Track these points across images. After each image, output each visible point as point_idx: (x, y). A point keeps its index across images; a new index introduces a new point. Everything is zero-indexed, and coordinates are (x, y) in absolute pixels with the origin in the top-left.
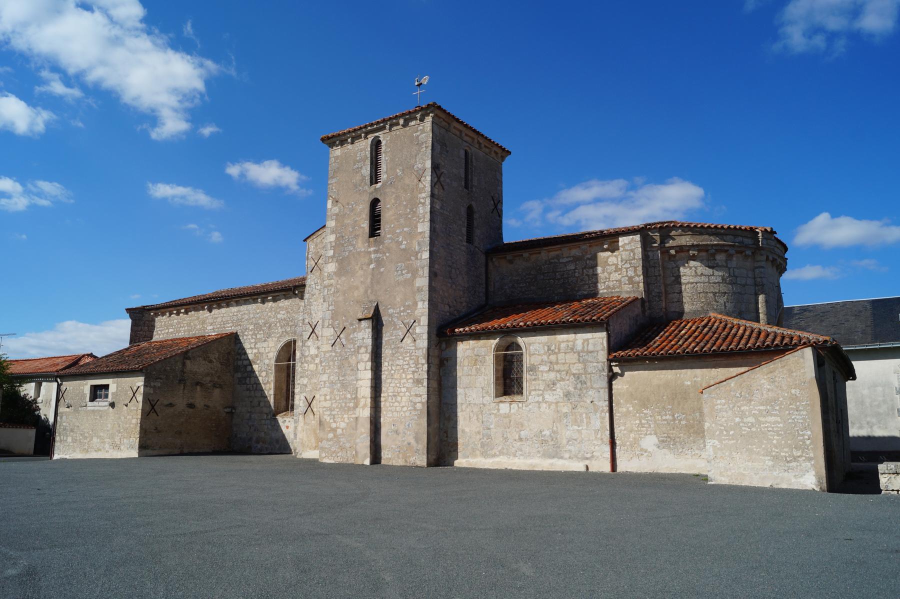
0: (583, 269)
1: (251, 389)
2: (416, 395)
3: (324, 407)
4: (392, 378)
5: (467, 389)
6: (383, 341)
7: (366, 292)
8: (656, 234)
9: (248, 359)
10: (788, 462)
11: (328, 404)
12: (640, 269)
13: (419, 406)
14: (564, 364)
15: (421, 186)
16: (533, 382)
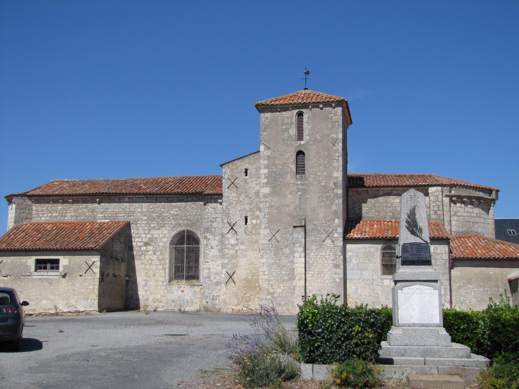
2: (336, 274)
4: (318, 263)
5: (362, 271)
7: (295, 209)
11: (267, 277)
13: (337, 280)
15: (335, 148)
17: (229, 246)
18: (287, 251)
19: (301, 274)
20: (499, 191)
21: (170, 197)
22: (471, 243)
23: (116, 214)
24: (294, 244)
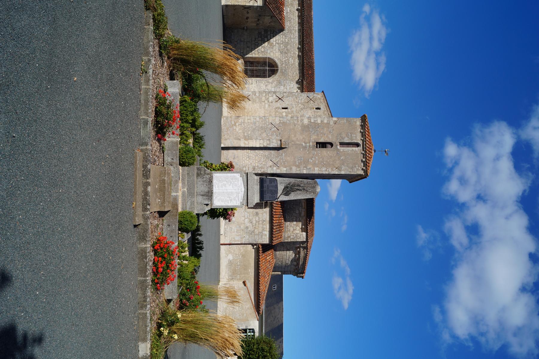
0: (296, 217)
1: (256, 41)
2: (249, 168)
3: (245, 119)
6: (271, 151)
7: (293, 141)
8: (306, 245)
10: (225, 312)
11: (246, 121)
12: (293, 240)
14: (258, 226)
16: (252, 214)
17: (267, 97)
18: (264, 135)
20: (303, 278)
21: (301, 58)
22: (269, 259)
24: (269, 140)
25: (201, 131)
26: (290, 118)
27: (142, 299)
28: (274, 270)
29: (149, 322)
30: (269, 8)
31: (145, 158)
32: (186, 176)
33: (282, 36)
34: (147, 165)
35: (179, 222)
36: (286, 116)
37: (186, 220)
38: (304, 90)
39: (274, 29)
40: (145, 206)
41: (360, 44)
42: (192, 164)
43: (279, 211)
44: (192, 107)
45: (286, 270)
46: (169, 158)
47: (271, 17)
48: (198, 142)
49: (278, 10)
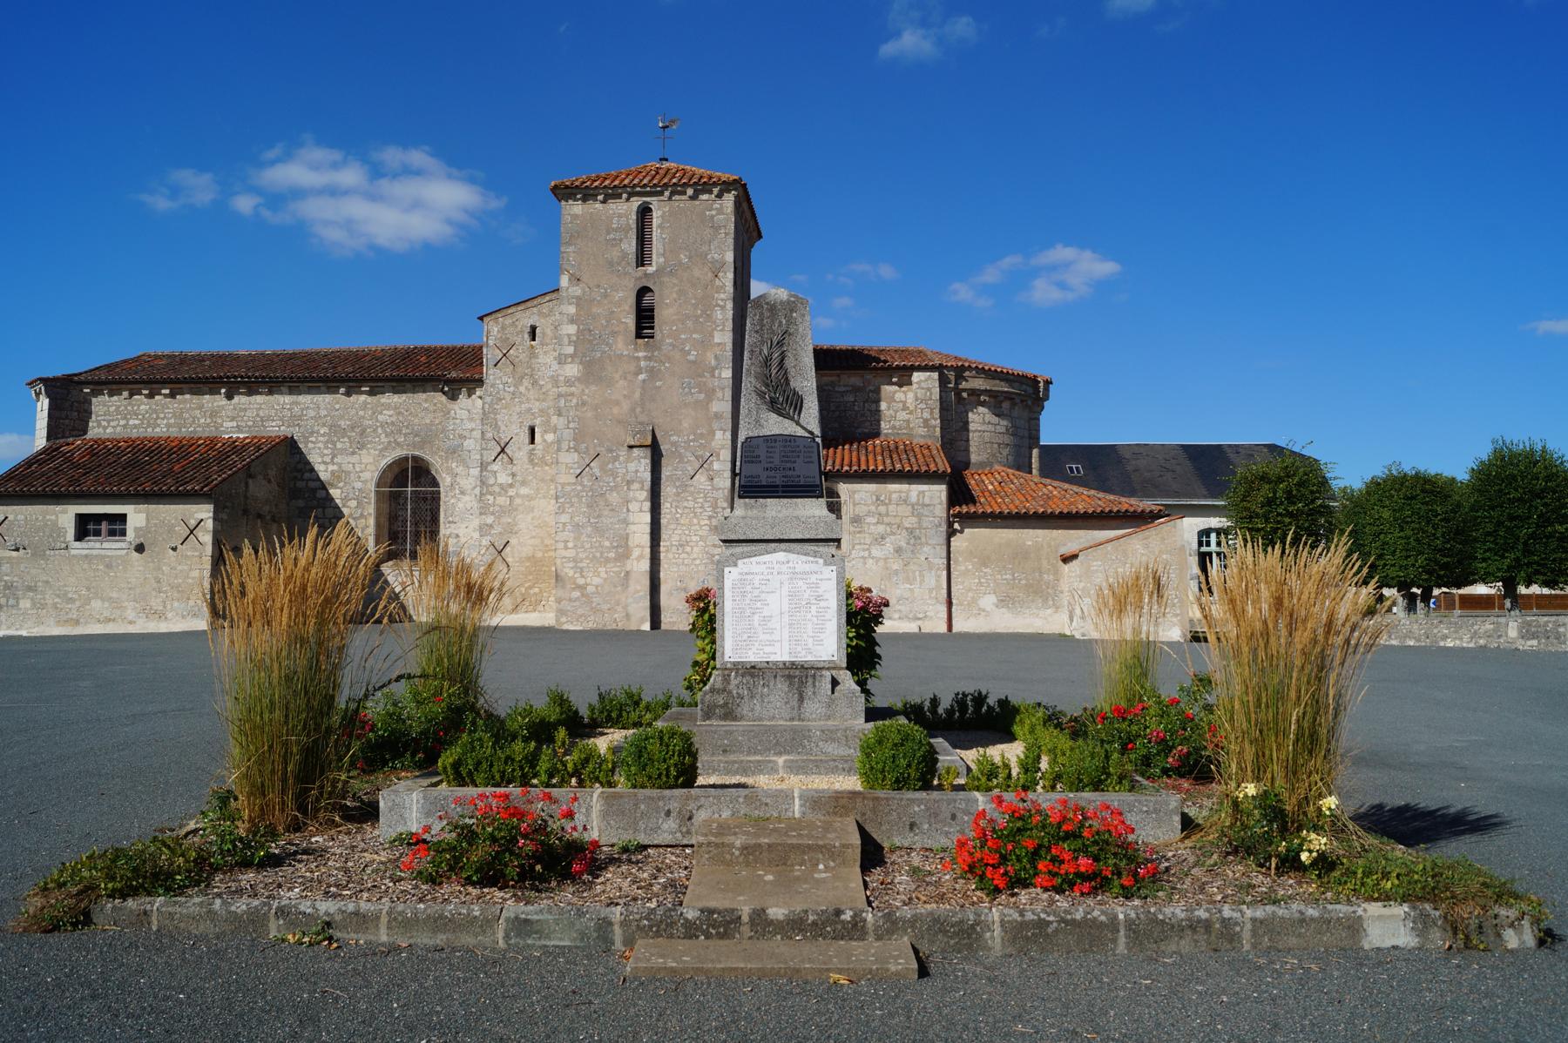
6: (663, 476)
7: (633, 410)
9: (318, 479)
11: (570, 553)
12: (937, 411)
17: (497, 489)
18: (614, 498)
19: (643, 547)
22: (992, 484)
23: (262, 421)
24: (629, 483)
25: (583, 702)
26: (561, 419)
27: (1201, 937)
28: (1027, 469)
29: (1286, 911)
30: (221, 482)
31: (657, 931)
32: (732, 757)
33: (310, 445)
34: (686, 920)
35: (899, 789)
36: (555, 433)
37: (893, 762)
38: (477, 377)
39: (288, 469)
40: (844, 928)
41: (349, 225)
42: (686, 738)
43: (846, 452)
44: (480, 739)
45: (1026, 434)
46: (665, 826)
47: (250, 476)
48: (621, 710)
49: (229, 456)
